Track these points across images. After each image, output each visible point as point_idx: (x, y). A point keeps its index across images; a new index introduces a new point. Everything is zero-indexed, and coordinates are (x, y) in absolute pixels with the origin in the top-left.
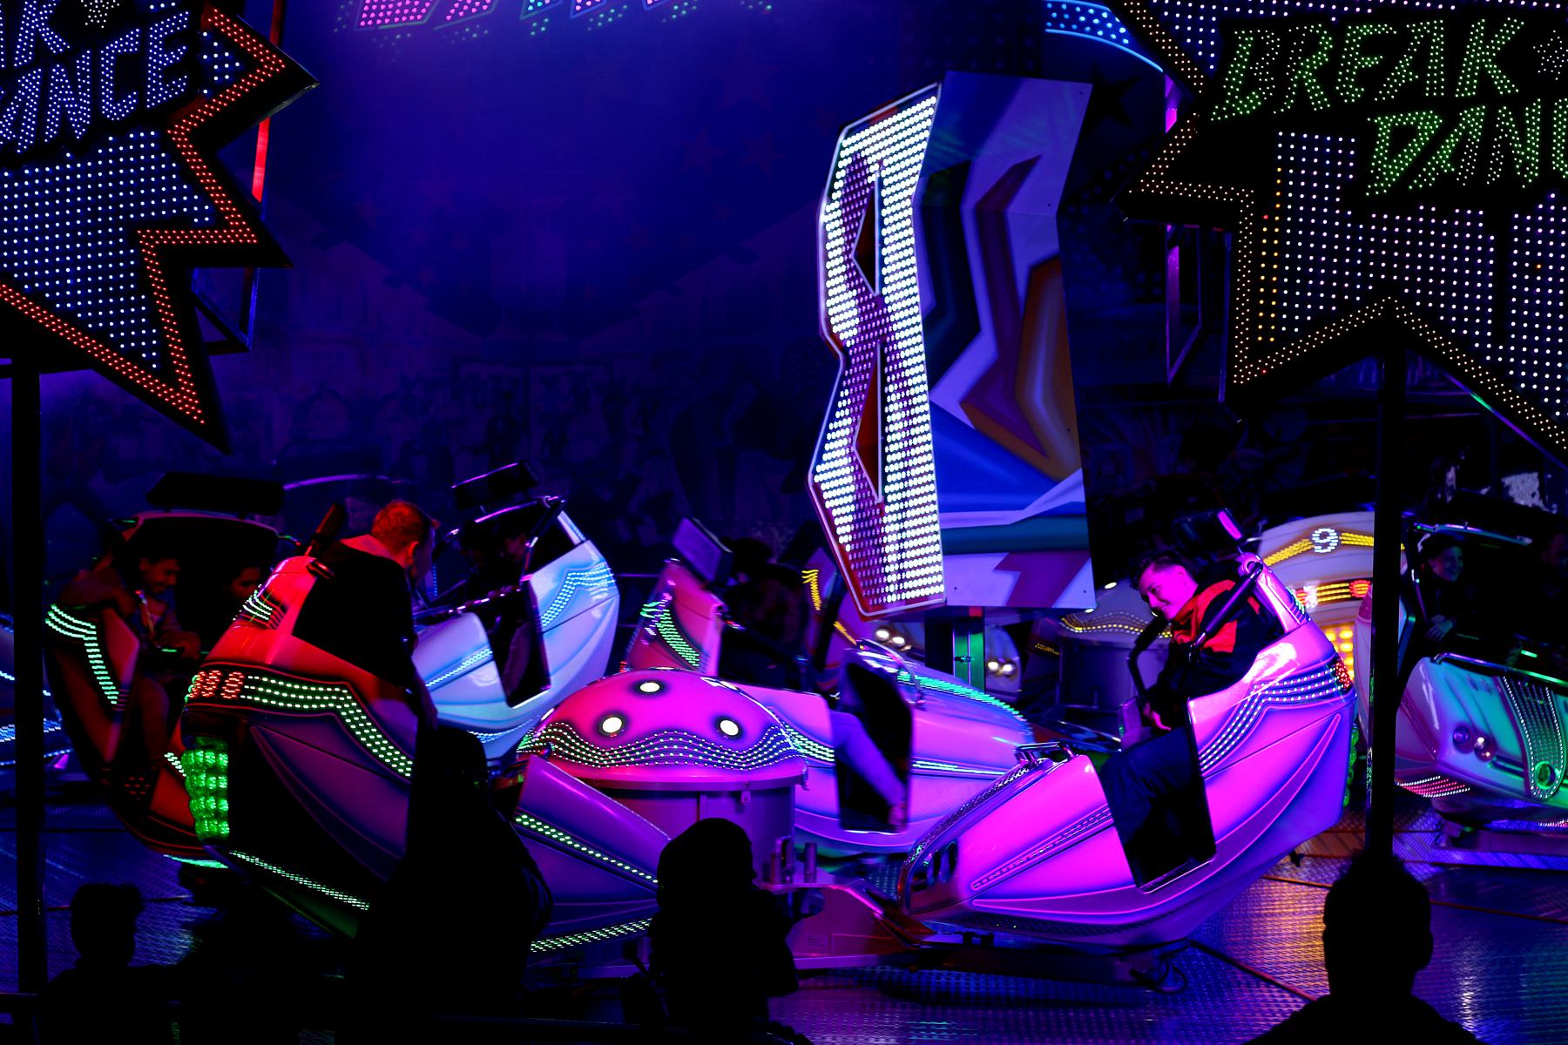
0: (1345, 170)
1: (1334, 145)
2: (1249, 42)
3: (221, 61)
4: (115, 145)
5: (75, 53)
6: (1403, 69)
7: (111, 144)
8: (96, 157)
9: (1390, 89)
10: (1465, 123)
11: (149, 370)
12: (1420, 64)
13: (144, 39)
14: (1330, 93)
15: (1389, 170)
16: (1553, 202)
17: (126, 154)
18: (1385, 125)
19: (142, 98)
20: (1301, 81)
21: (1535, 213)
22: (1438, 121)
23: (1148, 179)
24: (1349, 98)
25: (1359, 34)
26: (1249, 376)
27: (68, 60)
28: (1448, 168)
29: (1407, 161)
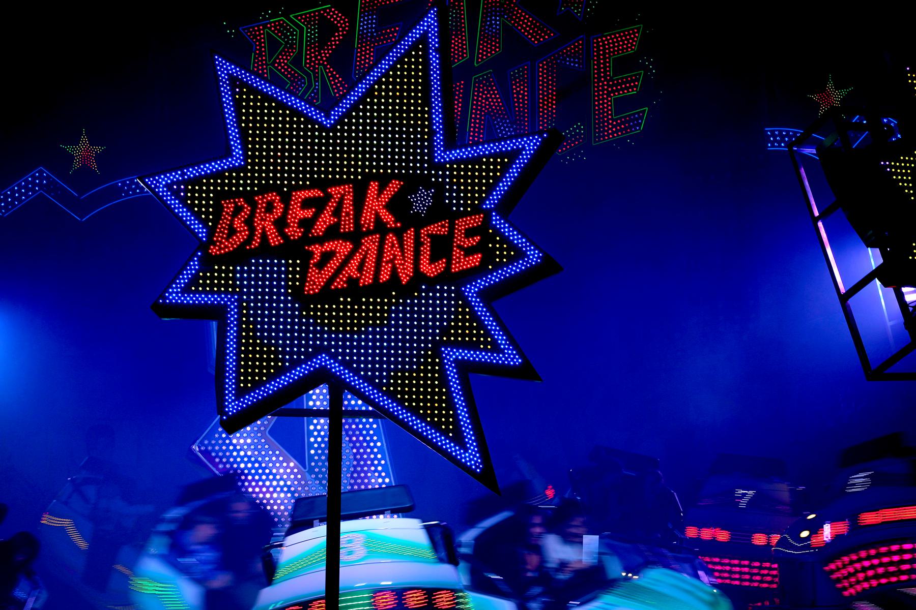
1: (287, 265)
2: (232, 207)
5: (404, 229)
6: (326, 219)
9: (320, 228)
10: (366, 246)
11: (447, 437)
12: (337, 212)
14: (282, 233)
16: (424, 291)
18: (317, 250)
20: (263, 228)
21: (293, 303)
22: (349, 246)
23: (170, 294)
24: (294, 236)
25: (300, 197)
26: (235, 409)
27: (399, 233)
28: (355, 274)
29: (330, 272)
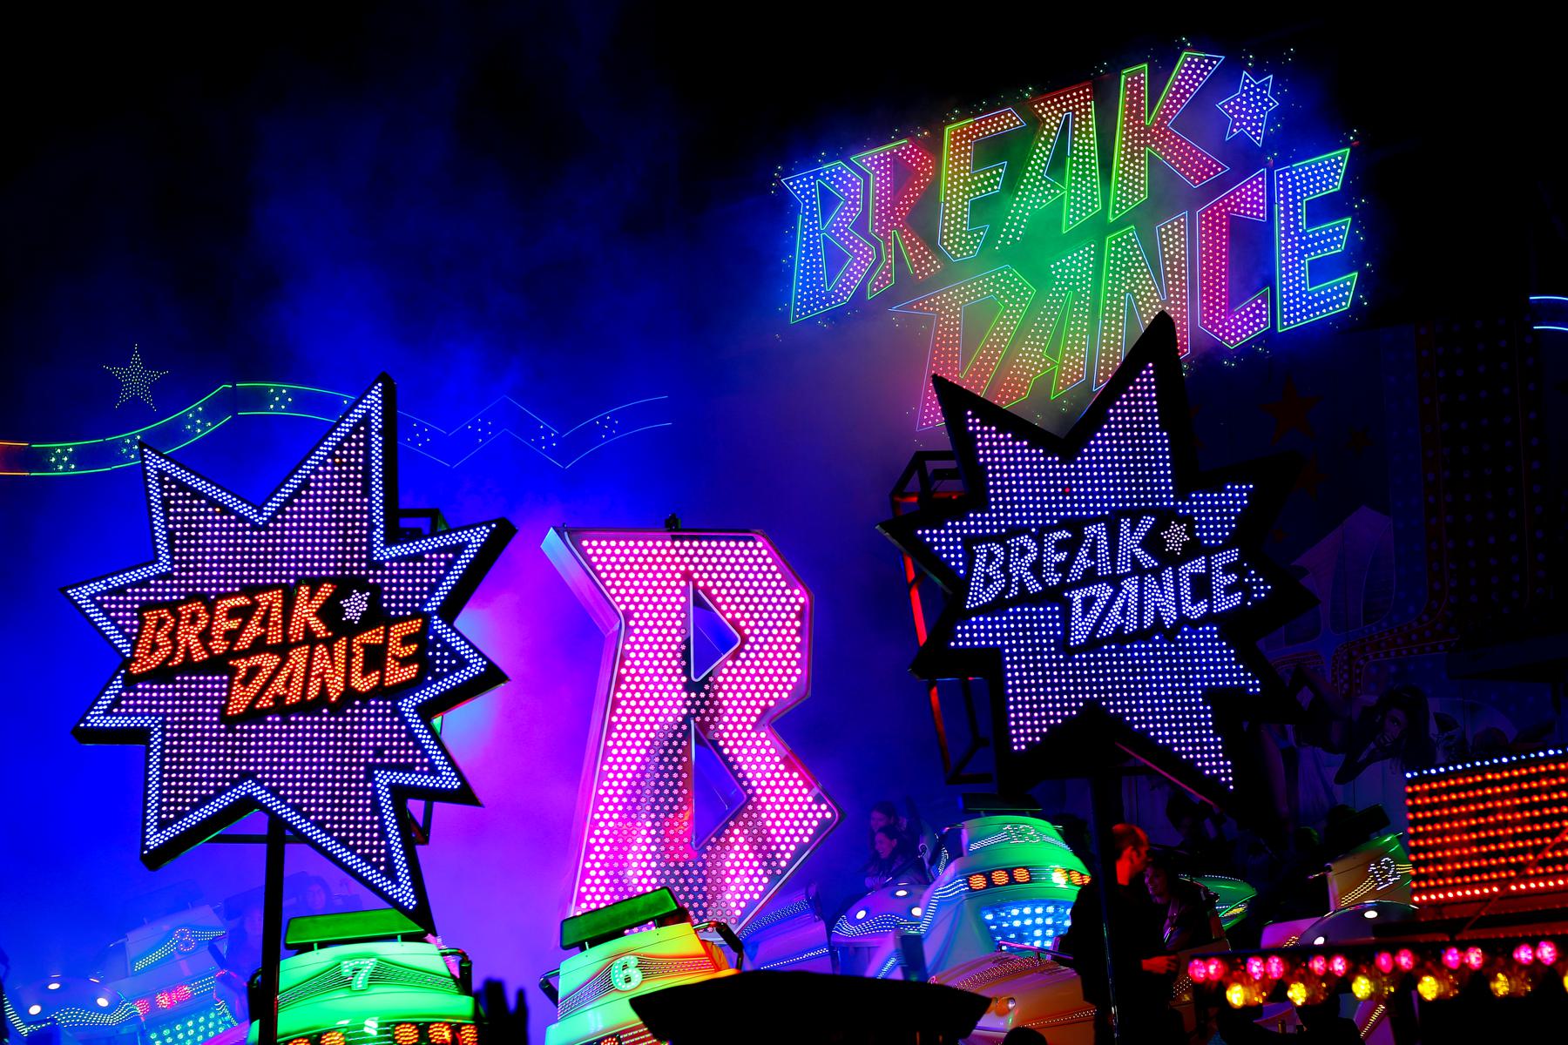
0: (1055, 629)
3: (442, 658)
4: (360, 708)
6: (254, 629)
7: (357, 707)
8: (345, 715)
9: (1076, 572)
12: (1092, 555)
13: (387, 633)
15: (1080, 631)
16: (1253, 576)
17: (368, 715)
18: (1077, 596)
19: (382, 677)
27: (329, 643)
